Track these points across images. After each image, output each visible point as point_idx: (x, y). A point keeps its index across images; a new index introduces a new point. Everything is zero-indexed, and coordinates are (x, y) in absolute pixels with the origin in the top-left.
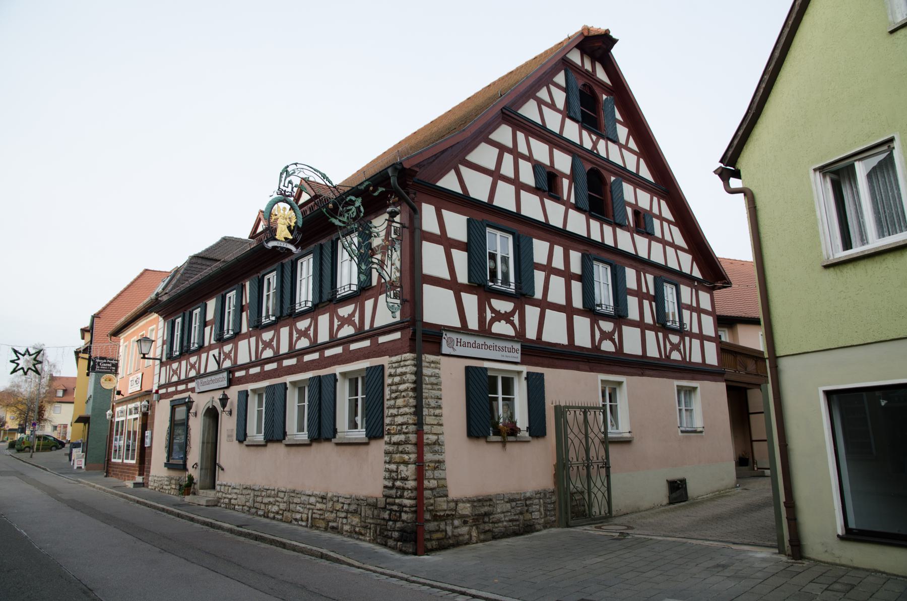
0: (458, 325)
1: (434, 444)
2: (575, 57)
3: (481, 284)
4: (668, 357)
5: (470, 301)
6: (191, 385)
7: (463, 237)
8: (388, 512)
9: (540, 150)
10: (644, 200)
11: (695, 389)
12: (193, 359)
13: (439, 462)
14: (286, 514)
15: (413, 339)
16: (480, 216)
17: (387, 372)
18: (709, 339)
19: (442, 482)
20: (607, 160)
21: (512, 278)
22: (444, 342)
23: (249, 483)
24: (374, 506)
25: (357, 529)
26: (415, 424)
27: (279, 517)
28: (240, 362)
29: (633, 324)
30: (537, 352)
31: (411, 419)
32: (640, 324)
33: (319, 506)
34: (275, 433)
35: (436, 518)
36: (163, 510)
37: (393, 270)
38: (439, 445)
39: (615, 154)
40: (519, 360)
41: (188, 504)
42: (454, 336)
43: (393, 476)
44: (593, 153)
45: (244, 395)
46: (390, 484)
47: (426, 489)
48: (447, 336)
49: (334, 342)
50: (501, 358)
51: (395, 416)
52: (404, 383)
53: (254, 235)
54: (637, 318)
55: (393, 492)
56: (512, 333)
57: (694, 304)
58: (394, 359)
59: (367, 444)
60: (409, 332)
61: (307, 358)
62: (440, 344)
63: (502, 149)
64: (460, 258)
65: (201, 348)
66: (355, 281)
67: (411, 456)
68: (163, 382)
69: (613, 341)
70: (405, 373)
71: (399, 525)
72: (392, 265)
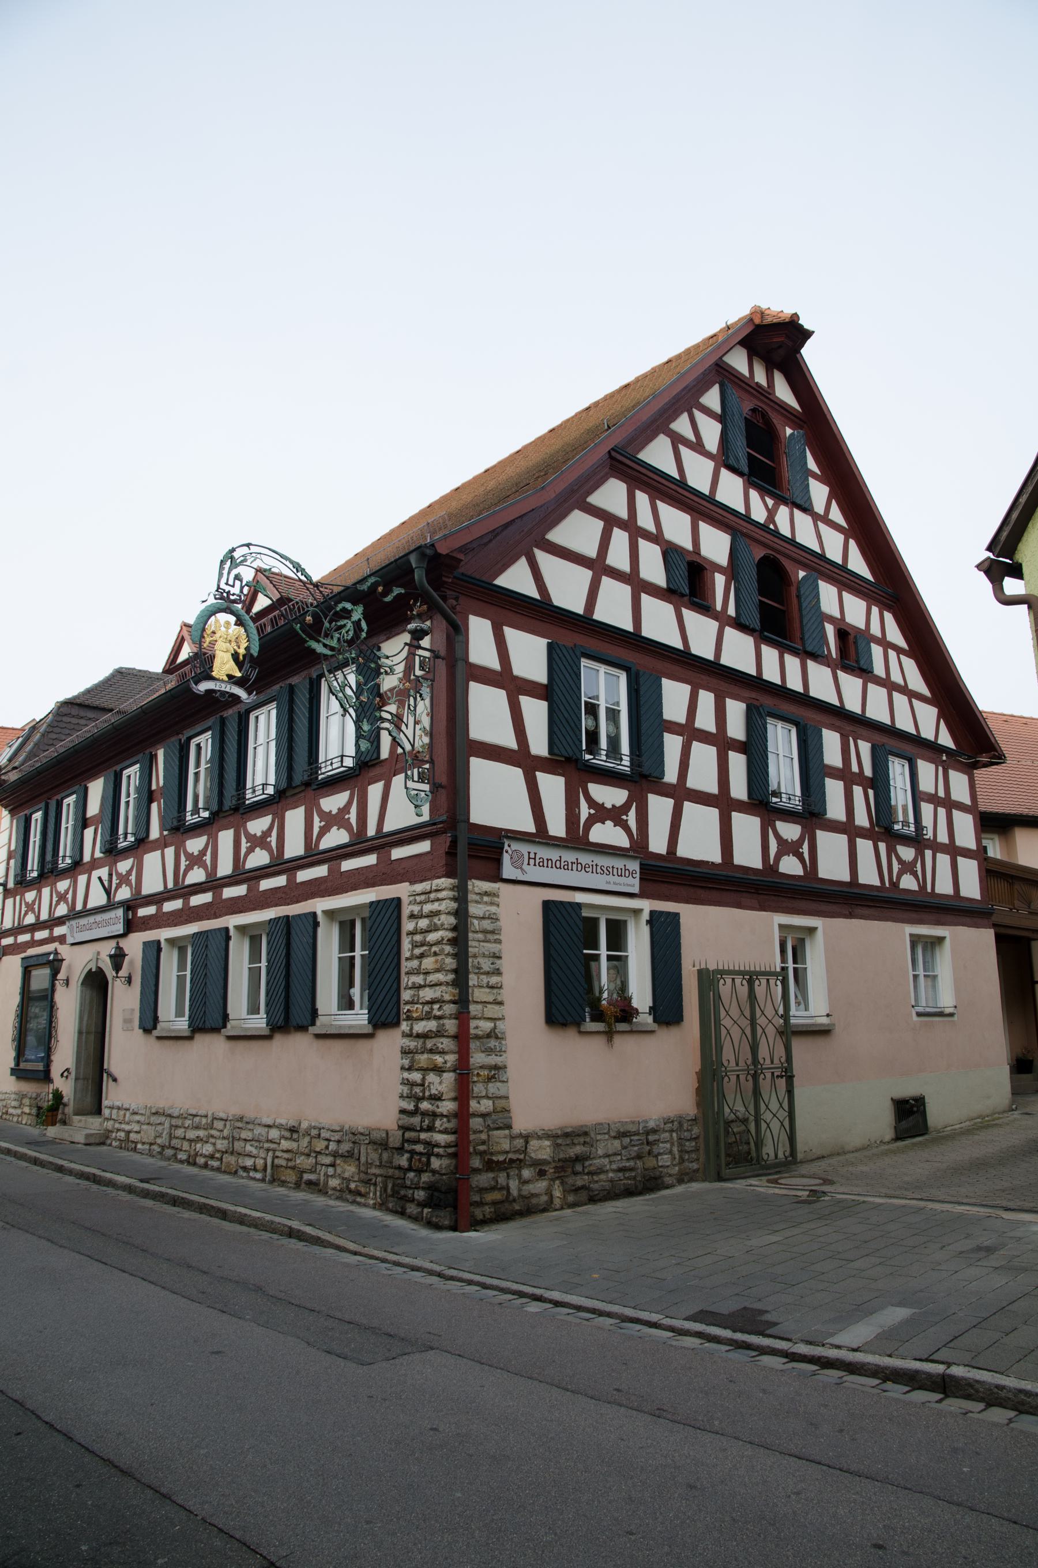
0: (531, 828)
1: (488, 1036)
2: (739, 361)
3: (571, 757)
4: (895, 885)
5: (553, 787)
6: (58, 931)
8: (407, 1156)
9: (677, 525)
10: (856, 611)
11: (941, 940)
12: (63, 885)
13: (496, 1067)
14: (228, 1158)
15: (452, 853)
16: (569, 639)
17: (406, 911)
18: (967, 853)
19: (500, 1104)
20: (792, 542)
21: (625, 748)
22: (506, 858)
23: (161, 1104)
24: (382, 1144)
25: (353, 1186)
26: (454, 1002)
27: (215, 1164)
28: (146, 890)
29: (834, 827)
30: (669, 876)
31: (448, 993)
32: (848, 828)
33: (285, 1144)
34: (208, 1017)
35: (490, 1165)
37: (418, 732)
38: (497, 1038)
40: (636, 890)
41: (53, 1142)
42: (524, 848)
43: (415, 1092)
44: (768, 529)
45: (154, 950)
46: (411, 1107)
47: (474, 1115)
48: (511, 848)
49: (312, 857)
50: (605, 887)
51: (421, 987)
52: (436, 930)
53: (172, 667)
55: (416, 1120)
56: (624, 842)
57: (941, 793)
58: (419, 887)
60: (446, 840)
61: (266, 884)
62: (498, 862)
63: (610, 521)
65: (77, 865)
66: (351, 750)
69: (800, 857)
70: (437, 913)
71: (425, 1177)
72: (416, 723)
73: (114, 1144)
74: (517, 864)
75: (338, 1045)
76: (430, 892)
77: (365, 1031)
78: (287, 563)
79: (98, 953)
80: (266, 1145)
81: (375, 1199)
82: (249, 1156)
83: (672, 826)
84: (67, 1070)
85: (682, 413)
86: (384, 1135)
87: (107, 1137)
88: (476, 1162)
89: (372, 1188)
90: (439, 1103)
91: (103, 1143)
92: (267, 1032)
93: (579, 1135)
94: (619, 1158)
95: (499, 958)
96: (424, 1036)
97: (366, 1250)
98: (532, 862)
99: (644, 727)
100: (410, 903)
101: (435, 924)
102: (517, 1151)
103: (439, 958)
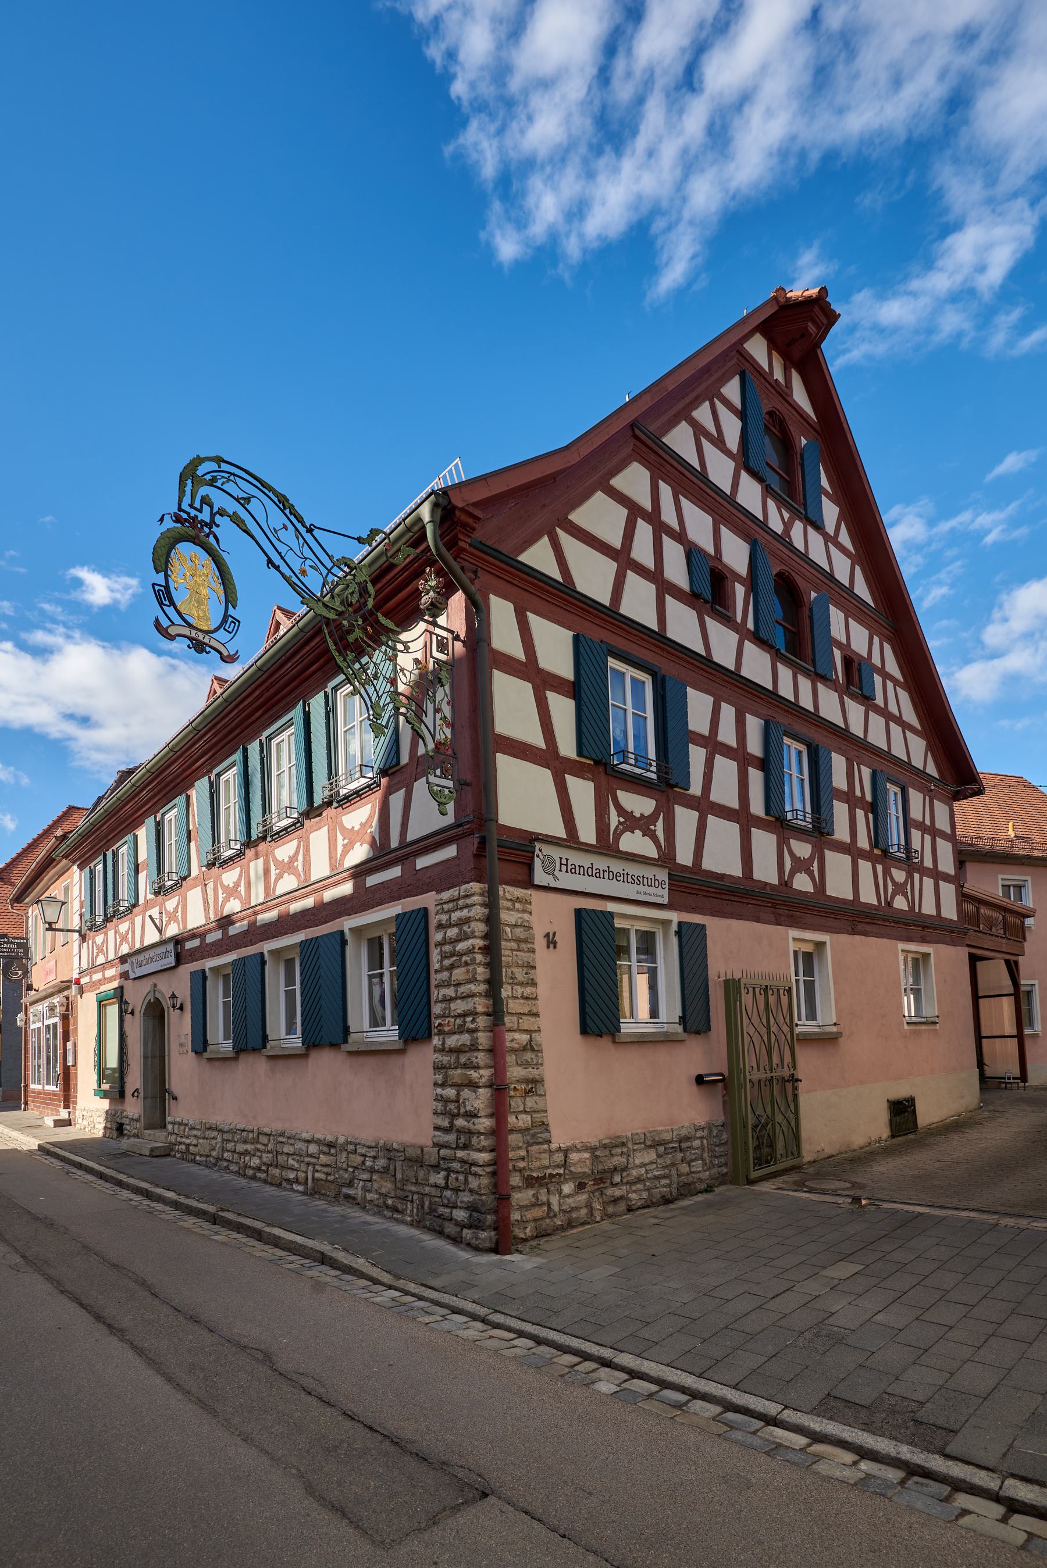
0: (562, 833)
1: (524, 1049)
2: (758, 349)
3: (597, 759)
4: (889, 904)
5: (582, 792)
7: (565, 669)
8: (443, 1174)
9: (699, 525)
10: (860, 639)
14: (276, 1172)
15: (480, 853)
16: (596, 633)
17: (433, 921)
18: (947, 878)
20: (805, 557)
21: (652, 754)
22: (537, 863)
24: (417, 1161)
25: (390, 1202)
26: (488, 1015)
27: (263, 1176)
29: (840, 847)
30: (694, 888)
31: (481, 1005)
32: (849, 849)
33: (324, 1159)
34: (250, 1039)
36: (80, 1166)
37: (438, 722)
38: (533, 1050)
39: (817, 552)
42: (556, 853)
43: (450, 1111)
45: (200, 979)
46: (446, 1124)
47: (512, 1131)
48: (543, 850)
50: (635, 898)
51: (452, 999)
52: (467, 938)
54: (847, 839)
55: (451, 1138)
56: (653, 853)
57: (928, 822)
58: (446, 895)
59: (401, 1052)
60: (473, 842)
62: (530, 867)
64: (563, 709)
67: (482, 1072)
68: (84, 966)
70: (467, 921)
71: (466, 1198)
72: (437, 710)
73: (178, 1155)
74: (549, 870)
75: (371, 1062)
76: (459, 899)
77: (397, 1047)
78: (271, 494)
79: (155, 985)
80: (307, 1159)
81: (412, 1216)
82: (292, 1169)
83: (697, 839)
84: (137, 1090)
85: (704, 401)
86: (419, 1152)
87: (172, 1150)
88: (515, 1180)
89: (409, 1205)
90: (476, 1120)
91: (169, 1155)
92: (303, 1051)
93: (616, 1146)
94: (654, 1166)
95: (535, 968)
96: (457, 1051)
97: (401, 1283)
98: (564, 868)
99: (670, 736)
100: (437, 913)
101: (465, 932)
102: (558, 1166)
103: (471, 968)
